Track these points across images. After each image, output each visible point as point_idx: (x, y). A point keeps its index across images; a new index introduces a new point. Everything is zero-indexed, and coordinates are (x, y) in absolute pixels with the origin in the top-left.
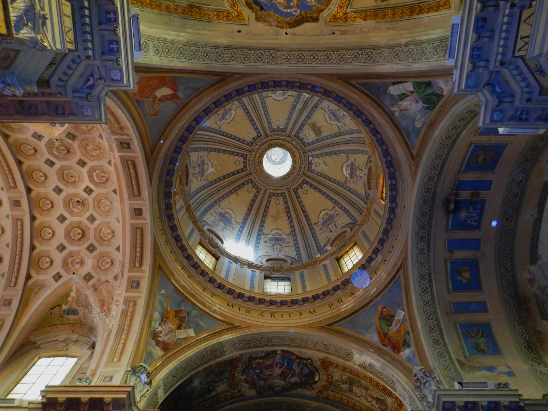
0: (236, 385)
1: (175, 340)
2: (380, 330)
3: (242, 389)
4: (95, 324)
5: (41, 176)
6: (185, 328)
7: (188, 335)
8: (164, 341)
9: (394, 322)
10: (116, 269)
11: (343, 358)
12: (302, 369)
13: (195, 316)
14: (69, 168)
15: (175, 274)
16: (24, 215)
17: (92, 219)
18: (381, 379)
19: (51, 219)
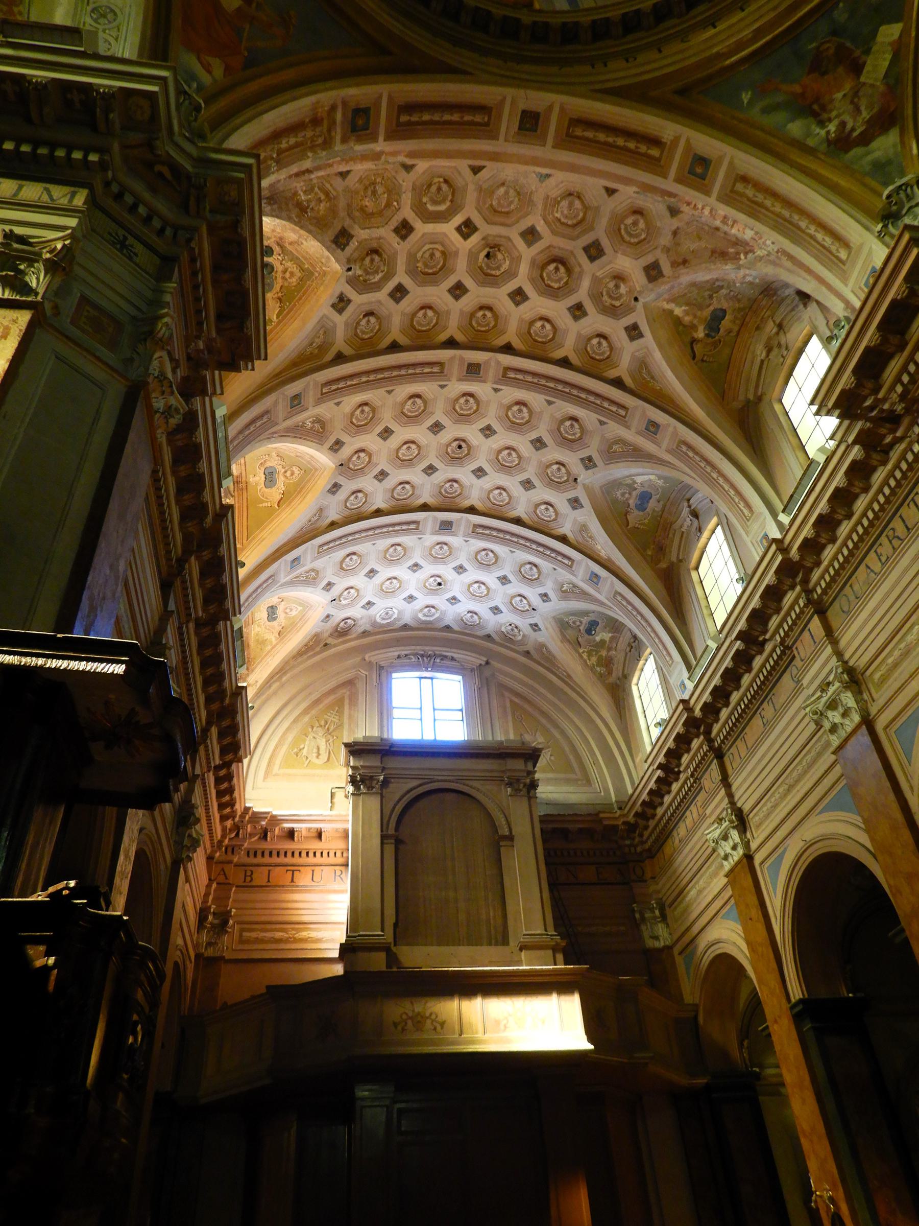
4: (757, 281)
5: (425, 315)
6: (868, 51)
7: (891, 44)
8: (868, 121)
10: (655, 206)
14: (412, 258)
15: (715, 50)
16: (498, 363)
17: (531, 235)
19: (515, 317)
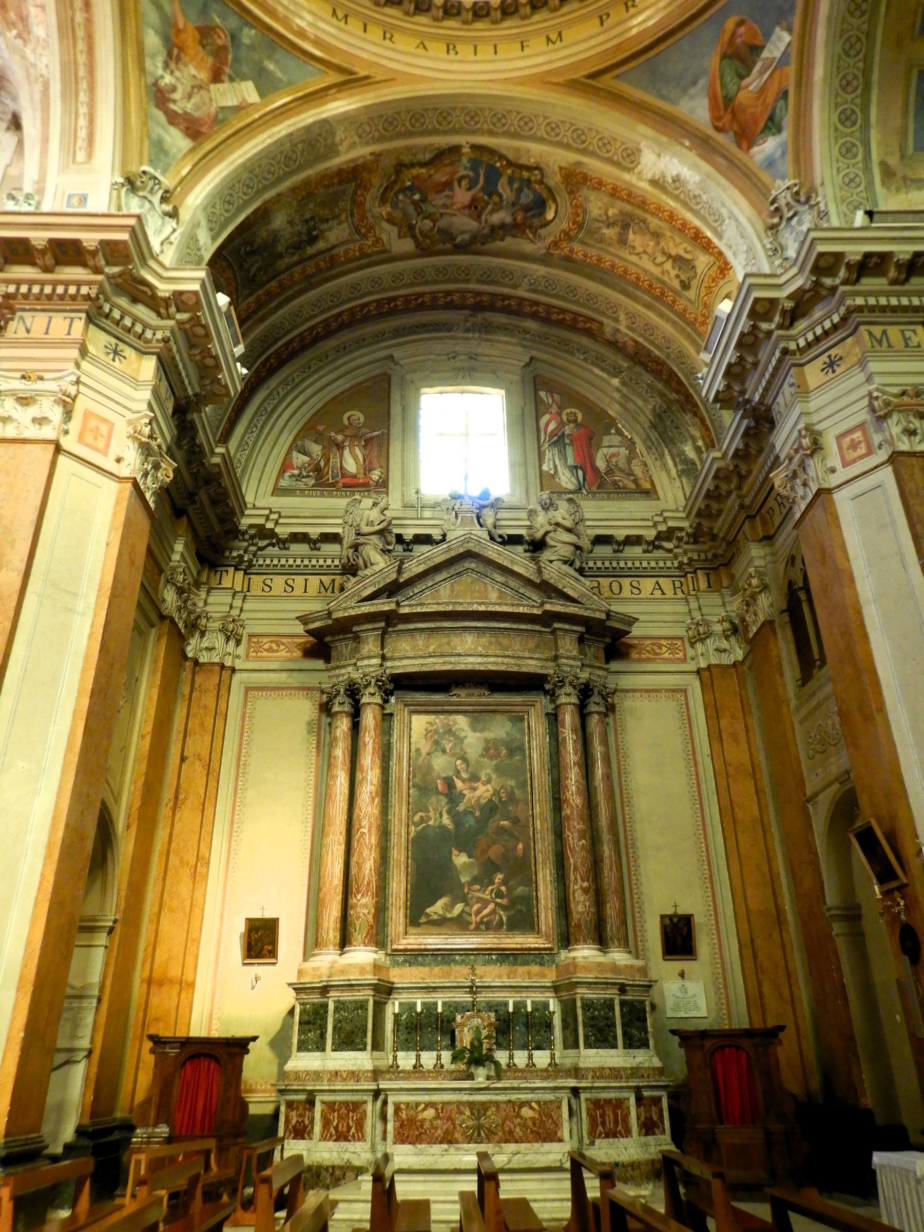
0: (370, 229)
1: (213, 110)
2: (719, 89)
3: (384, 237)
6: (232, 80)
7: (244, 100)
8: (186, 113)
9: (759, 65)
11: (617, 164)
12: (520, 191)
13: (251, 47)
18: (696, 213)
